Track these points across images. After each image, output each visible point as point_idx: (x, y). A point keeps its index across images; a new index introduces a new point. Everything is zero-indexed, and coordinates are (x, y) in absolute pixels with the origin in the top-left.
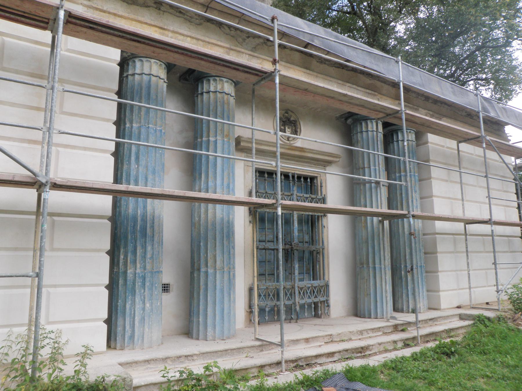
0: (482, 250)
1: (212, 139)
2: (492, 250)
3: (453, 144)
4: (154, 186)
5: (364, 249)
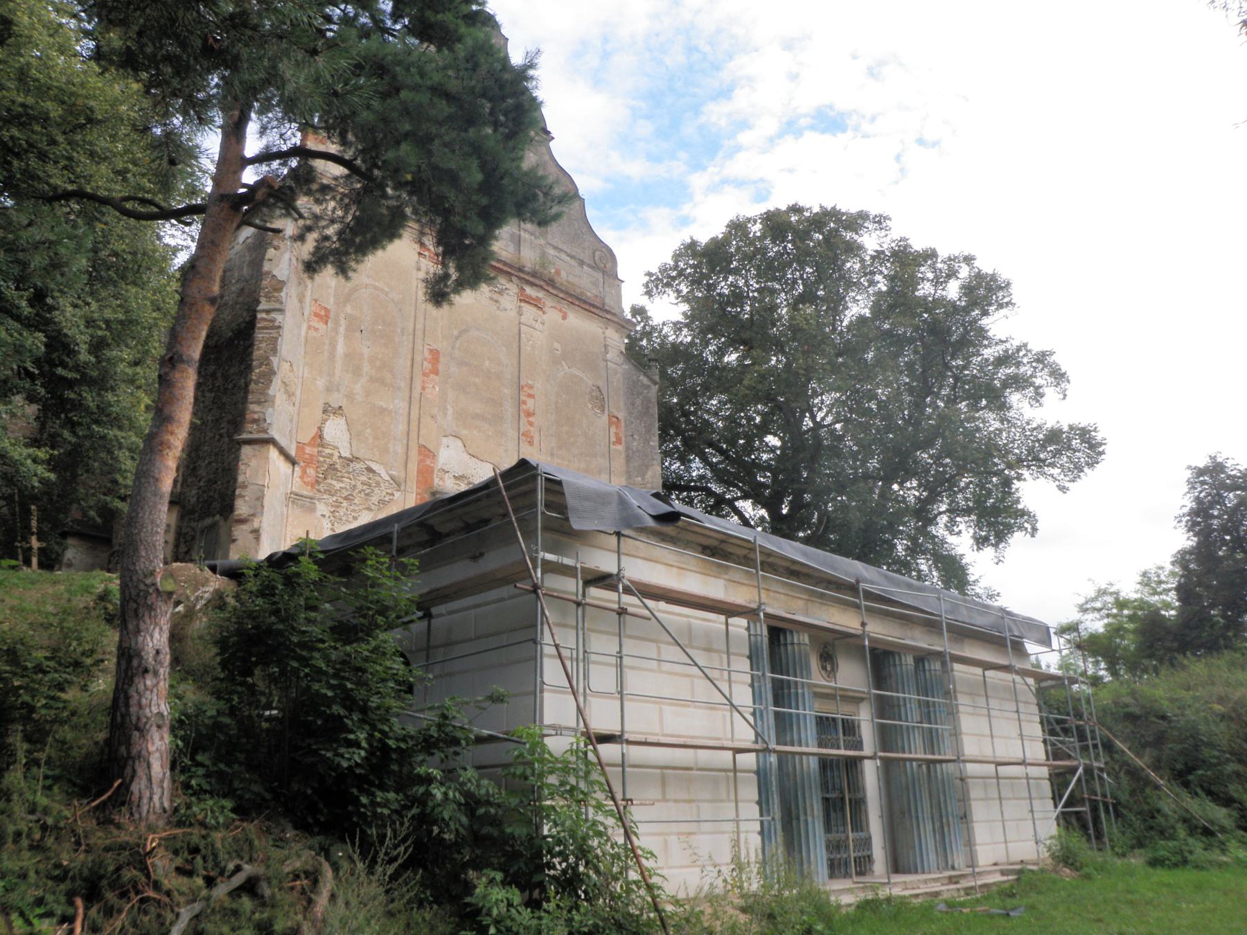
0: (1011, 796)
1: (800, 691)
2: (1028, 795)
3: (979, 671)
4: (945, 754)
5: (905, 798)
